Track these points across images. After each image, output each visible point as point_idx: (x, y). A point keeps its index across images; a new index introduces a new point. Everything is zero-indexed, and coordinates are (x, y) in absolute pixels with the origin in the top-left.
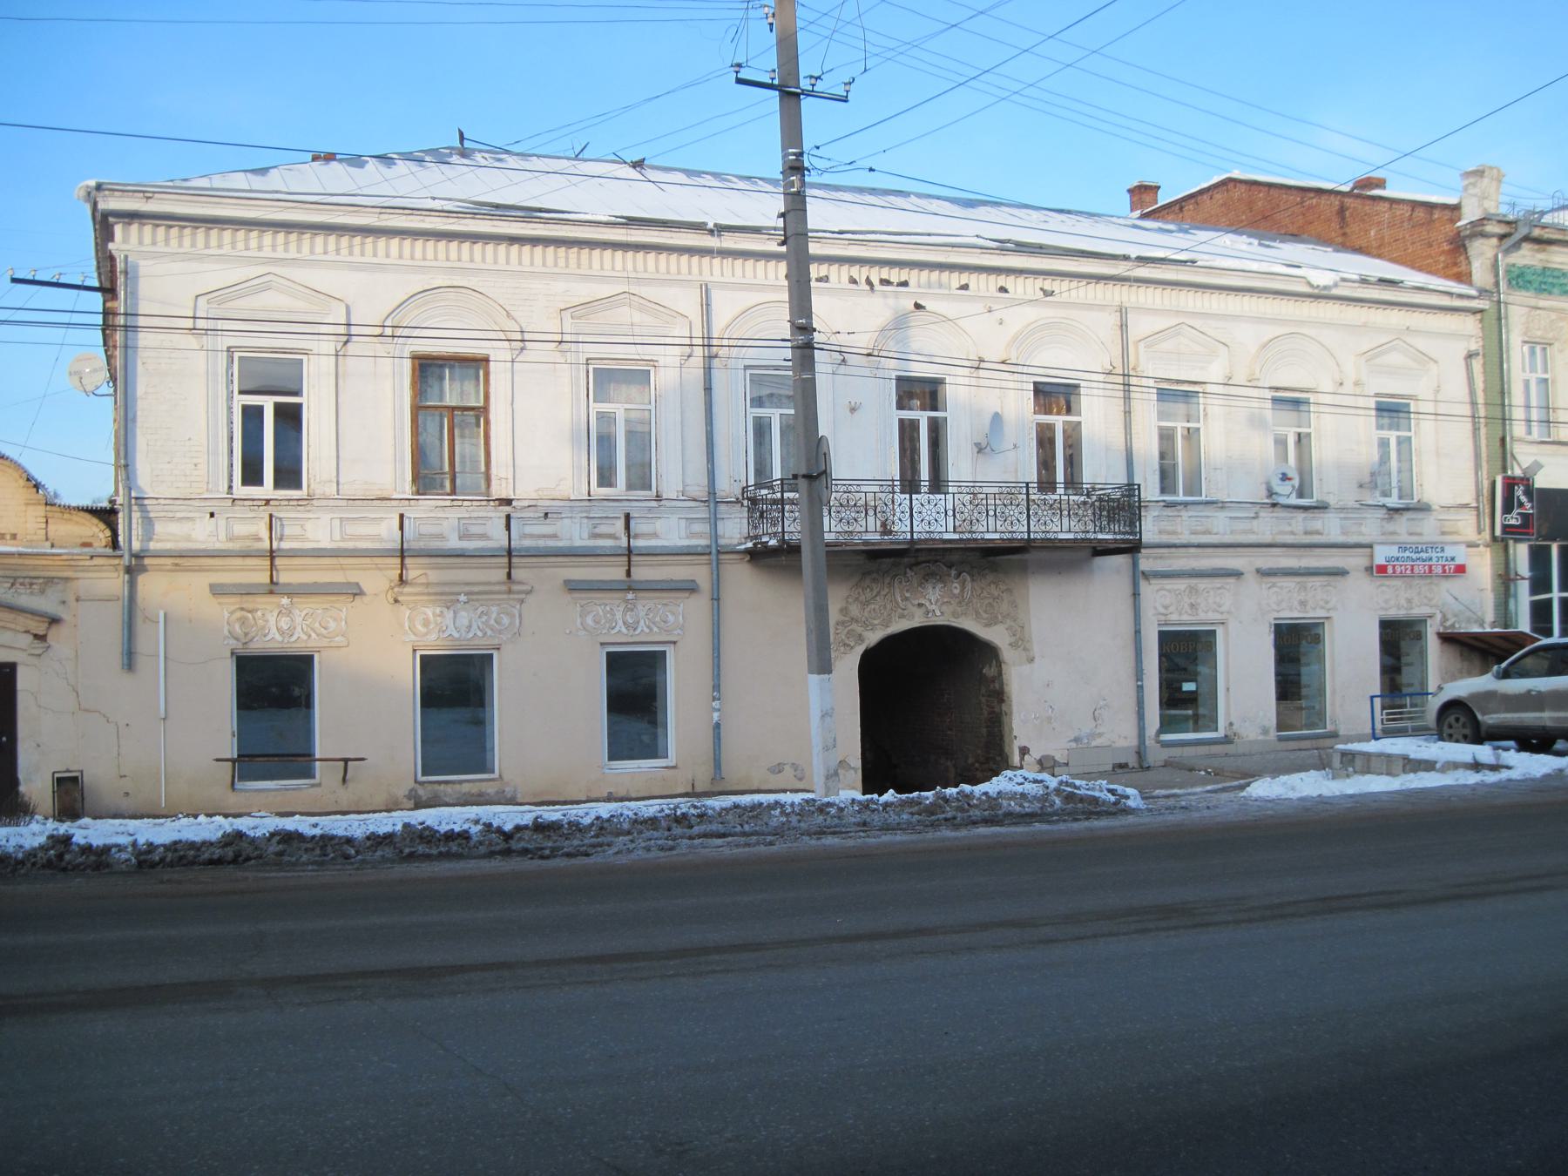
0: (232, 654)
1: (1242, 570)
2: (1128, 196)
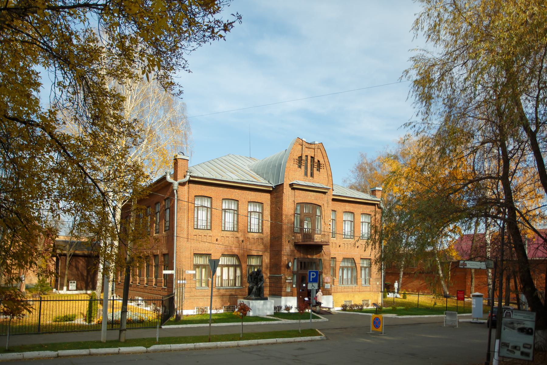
2: (293, 139)
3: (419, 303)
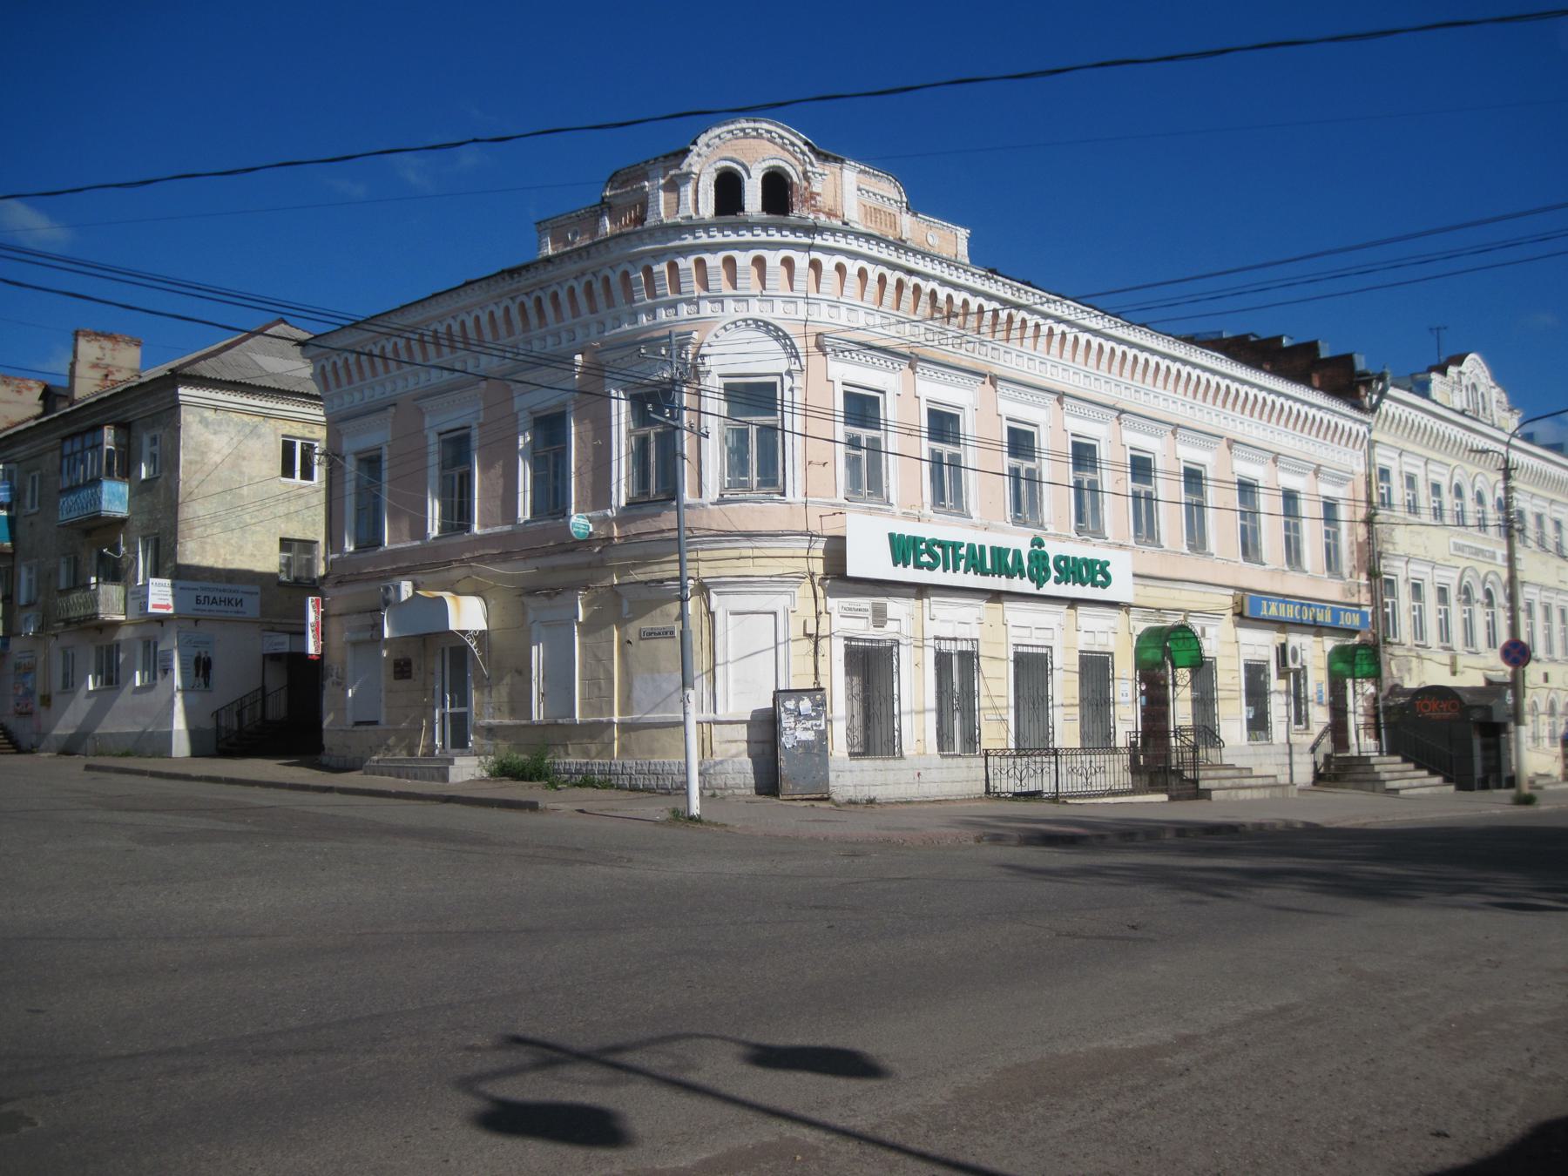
0: (1431, 329)
1: (885, 1063)
3: (1188, 664)
